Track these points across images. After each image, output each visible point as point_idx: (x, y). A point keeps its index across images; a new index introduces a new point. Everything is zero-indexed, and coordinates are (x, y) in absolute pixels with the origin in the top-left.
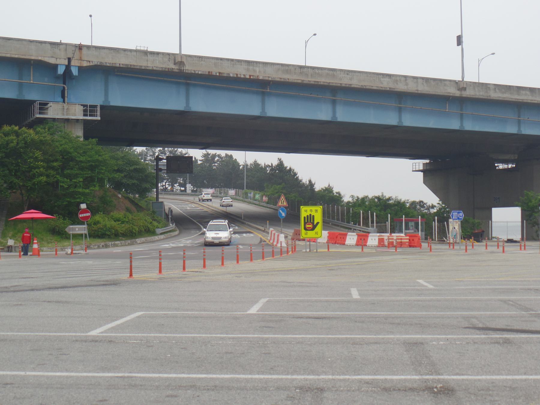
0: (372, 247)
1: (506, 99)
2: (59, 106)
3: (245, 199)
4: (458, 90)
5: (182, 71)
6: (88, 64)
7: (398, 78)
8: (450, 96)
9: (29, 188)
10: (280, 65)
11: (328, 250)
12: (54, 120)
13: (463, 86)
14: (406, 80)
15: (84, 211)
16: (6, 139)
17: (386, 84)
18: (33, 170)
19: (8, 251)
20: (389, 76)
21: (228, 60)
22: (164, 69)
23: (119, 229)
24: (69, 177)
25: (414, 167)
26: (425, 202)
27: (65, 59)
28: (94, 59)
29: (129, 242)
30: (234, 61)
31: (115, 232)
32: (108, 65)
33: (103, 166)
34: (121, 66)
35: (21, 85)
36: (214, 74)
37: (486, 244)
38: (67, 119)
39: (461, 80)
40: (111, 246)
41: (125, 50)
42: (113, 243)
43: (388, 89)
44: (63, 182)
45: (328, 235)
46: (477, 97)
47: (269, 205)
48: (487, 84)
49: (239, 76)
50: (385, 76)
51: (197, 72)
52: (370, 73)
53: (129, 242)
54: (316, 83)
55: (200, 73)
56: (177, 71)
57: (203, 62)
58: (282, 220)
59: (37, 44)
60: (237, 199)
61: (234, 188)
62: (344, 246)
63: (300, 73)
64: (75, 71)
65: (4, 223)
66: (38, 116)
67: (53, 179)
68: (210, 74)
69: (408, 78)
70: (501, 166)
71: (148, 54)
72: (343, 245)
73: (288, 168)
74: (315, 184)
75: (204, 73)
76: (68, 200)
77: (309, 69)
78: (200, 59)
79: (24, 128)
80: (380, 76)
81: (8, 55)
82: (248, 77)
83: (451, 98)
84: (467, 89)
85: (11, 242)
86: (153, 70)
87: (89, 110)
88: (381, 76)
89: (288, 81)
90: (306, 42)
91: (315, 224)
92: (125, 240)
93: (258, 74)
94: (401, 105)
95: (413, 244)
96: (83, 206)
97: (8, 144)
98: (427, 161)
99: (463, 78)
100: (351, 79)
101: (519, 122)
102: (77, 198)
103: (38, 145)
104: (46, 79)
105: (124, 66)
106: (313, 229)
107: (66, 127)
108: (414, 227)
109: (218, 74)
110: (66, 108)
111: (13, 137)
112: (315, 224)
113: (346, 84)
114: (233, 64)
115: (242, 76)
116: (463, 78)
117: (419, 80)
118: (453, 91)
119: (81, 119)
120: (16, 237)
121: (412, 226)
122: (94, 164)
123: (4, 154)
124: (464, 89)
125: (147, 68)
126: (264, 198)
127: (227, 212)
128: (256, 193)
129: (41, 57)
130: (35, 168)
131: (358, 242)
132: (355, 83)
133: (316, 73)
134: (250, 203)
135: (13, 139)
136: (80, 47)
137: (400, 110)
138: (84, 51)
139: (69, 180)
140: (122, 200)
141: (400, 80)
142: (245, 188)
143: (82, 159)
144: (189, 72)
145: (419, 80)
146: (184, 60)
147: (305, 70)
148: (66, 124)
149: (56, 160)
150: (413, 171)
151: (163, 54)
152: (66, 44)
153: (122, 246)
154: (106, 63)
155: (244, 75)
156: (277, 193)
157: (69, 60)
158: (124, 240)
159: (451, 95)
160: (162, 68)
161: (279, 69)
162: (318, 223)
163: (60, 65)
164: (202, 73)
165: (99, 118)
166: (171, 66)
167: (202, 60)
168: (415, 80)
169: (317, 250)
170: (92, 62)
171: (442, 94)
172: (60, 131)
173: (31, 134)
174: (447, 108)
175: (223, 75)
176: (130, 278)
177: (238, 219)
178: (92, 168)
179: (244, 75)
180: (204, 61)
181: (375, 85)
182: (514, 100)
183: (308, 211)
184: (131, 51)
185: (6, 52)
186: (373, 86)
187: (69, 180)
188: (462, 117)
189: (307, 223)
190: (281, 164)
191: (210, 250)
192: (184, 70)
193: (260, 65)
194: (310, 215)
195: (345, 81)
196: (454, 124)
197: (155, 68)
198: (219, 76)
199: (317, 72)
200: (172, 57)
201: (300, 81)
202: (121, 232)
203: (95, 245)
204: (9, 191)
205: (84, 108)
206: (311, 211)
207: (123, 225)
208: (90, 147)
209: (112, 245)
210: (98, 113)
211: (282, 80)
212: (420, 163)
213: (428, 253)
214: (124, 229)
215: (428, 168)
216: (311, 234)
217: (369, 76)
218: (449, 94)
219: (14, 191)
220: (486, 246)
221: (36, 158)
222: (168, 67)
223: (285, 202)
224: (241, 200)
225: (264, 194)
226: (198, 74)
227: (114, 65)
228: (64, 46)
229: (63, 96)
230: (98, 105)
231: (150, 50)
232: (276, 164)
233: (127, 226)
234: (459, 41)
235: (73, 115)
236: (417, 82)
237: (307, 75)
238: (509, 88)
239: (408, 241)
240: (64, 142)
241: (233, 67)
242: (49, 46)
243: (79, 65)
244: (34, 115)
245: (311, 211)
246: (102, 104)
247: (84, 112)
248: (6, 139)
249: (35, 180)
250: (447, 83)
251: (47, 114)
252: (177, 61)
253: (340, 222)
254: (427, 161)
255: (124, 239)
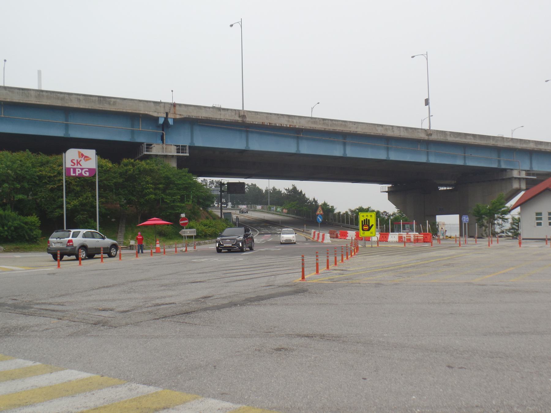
0: (392, 242)
1: (457, 142)
2: (160, 146)
3: (269, 211)
4: (427, 135)
5: (244, 122)
6: (180, 117)
7: (388, 127)
8: (421, 140)
9: (142, 203)
10: (310, 118)
11: (378, 245)
12: (156, 156)
13: (430, 133)
14: (393, 129)
15: (184, 219)
16: (125, 168)
17: (380, 131)
18: (145, 190)
19: (131, 249)
20: (382, 126)
21: (275, 114)
22: (232, 121)
23: (207, 232)
24: (170, 194)
25: (382, 189)
26: (387, 212)
27: (164, 113)
28: (185, 114)
29: (214, 241)
30: (279, 115)
31: (205, 234)
32: (194, 117)
33: (194, 187)
34: (203, 118)
35: (133, 132)
36: (266, 124)
37: (498, 240)
38: (165, 155)
39: (429, 129)
40: (202, 244)
41: (205, 107)
42: (204, 241)
43: (381, 135)
44: (166, 199)
45: (355, 234)
46: (439, 140)
47: (288, 215)
48: (445, 132)
49: (283, 125)
50: (379, 126)
51: (254, 123)
52: (369, 124)
53: (214, 241)
54: (334, 130)
55: (256, 123)
56: (241, 122)
57: (258, 116)
58: (319, 224)
59: (145, 103)
60: (263, 212)
61: (260, 204)
62: (369, 242)
63: (323, 123)
64: (171, 122)
65: (124, 229)
66: (146, 153)
67: (159, 197)
68: (263, 124)
69: (394, 127)
70: (442, 188)
71: (221, 110)
72: (368, 241)
73: (300, 191)
74: (317, 201)
75: (259, 123)
76: (170, 211)
77: (329, 121)
78: (257, 113)
79: (137, 161)
80: (376, 126)
81: (125, 111)
82: (288, 126)
83: (422, 141)
84: (432, 135)
85: (132, 242)
86: (224, 121)
87: (181, 149)
88: (377, 125)
89: (315, 129)
90: (312, 109)
91: (370, 226)
92: (211, 239)
93: (295, 124)
94: (388, 145)
95: (427, 241)
96: (183, 215)
97: (126, 172)
98: (390, 185)
99: (430, 127)
100: (357, 128)
101: (465, 158)
102: (176, 210)
103: (150, 172)
104: (150, 128)
105: (205, 118)
106: (369, 230)
107: (165, 161)
108: (409, 228)
109: (268, 124)
110: (164, 148)
111: (130, 167)
112: (370, 226)
113: (353, 131)
114: (279, 118)
115: (285, 126)
116: (430, 127)
117: (402, 129)
118: (423, 136)
119: (175, 155)
120: (134, 238)
121: (408, 227)
122: (187, 186)
123: (124, 179)
124: (431, 135)
125: (221, 120)
126: (284, 211)
127: (264, 220)
128: (278, 207)
129: (147, 111)
130: (146, 189)
131: (381, 239)
132: (359, 130)
133: (334, 123)
134: (273, 214)
135: (130, 169)
136: (174, 105)
137: (388, 149)
138: (177, 108)
139: (170, 197)
140: (202, 211)
141: (389, 128)
142: (269, 204)
143: (179, 182)
144: (249, 122)
145: (402, 129)
146: (246, 114)
147: (326, 121)
148: (165, 159)
149: (161, 183)
150: (381, 192)
151: (231, 110)
152: (165, 103)
153: (210, 244)
154: (192, 116)
155: (286, 125)
156: (294, 207)
157: (167, 114)
158: (210, 239)
159: (422, 139)
160: (231, 120)
161: (309, 121)
162: (372, 225)
163: (161, 117)
164: (258, 123)
165: (188, 155)
166: (237, 118)
167: (257, 115)
168: (399, 129)
169: (372, 246)
170: (183, 115)
171: (416, 138)
172: (161, 164)
173: (143, 164)
174: (419, 147)
175: (271, 125)
176: (303, 280)
177: (277, 224)
178: (186, 188)
179: (286, 125)
180: (259, 115)
181: (372, 132)
182: (463, 142)
183: (365, 216)
184: (209, 108)
185: (123, 108)
186: (371, 133)
187: (170, 197)
188: (428, 154)
189: (364, 225)
190: (295, 188)
191: (289, 247)
192: (245, 121)
193: (297, 118)
194: (367, 219)
195: (353, 129)
196: (422, 159)
197: (226, 120)
198: (269, 125)
199: (334, 123)
200: (238, 112)
201: (323, 129)
202: (209, 233)
203: (192, 243)
204: (128, 206)
205: (177, 148)
206: (367, 216)
207: (210, 229)
208: (184, 174)
209: (203, 243)
210: (187, 151)
211: (311, 128)
212: (386, 187)
213: (458, 248)
214: (211, 231)
215: (391, 190)
216: (367, 234)
217: (369, 125)
218: (421, 138)
219: (131, 205)
220: (498, 241)
221: (147, 181)
222: (235, 119)
223: (321, 211)
224: (266, 212)
225: (285, 208)
226: (255, 124)
227: (198, 118)
228: (163, 104)
229: (162, 140)
230: (187, 146)
231: (223, 107)
232: (292, 188)
233: (213, 229)
234: (427, 102)
235: (169, 153)
236: (400, 130)
237: (328, 125)
238: (459, 134)
239: (422, 238)
240: (165, 170)
241: (279, 119)
242: (152, 104)
243: (174, 117)
244: (142, 153)
245: (367, 216)
246: (189, 145)
247: (177, 150)
248: (125, 168)
249: (147, 197)
250: (420, 131)
251: (151, 151)
252: (241, 115)
253: (350, 225)
254: (390, 185)
255: (210, 239)
